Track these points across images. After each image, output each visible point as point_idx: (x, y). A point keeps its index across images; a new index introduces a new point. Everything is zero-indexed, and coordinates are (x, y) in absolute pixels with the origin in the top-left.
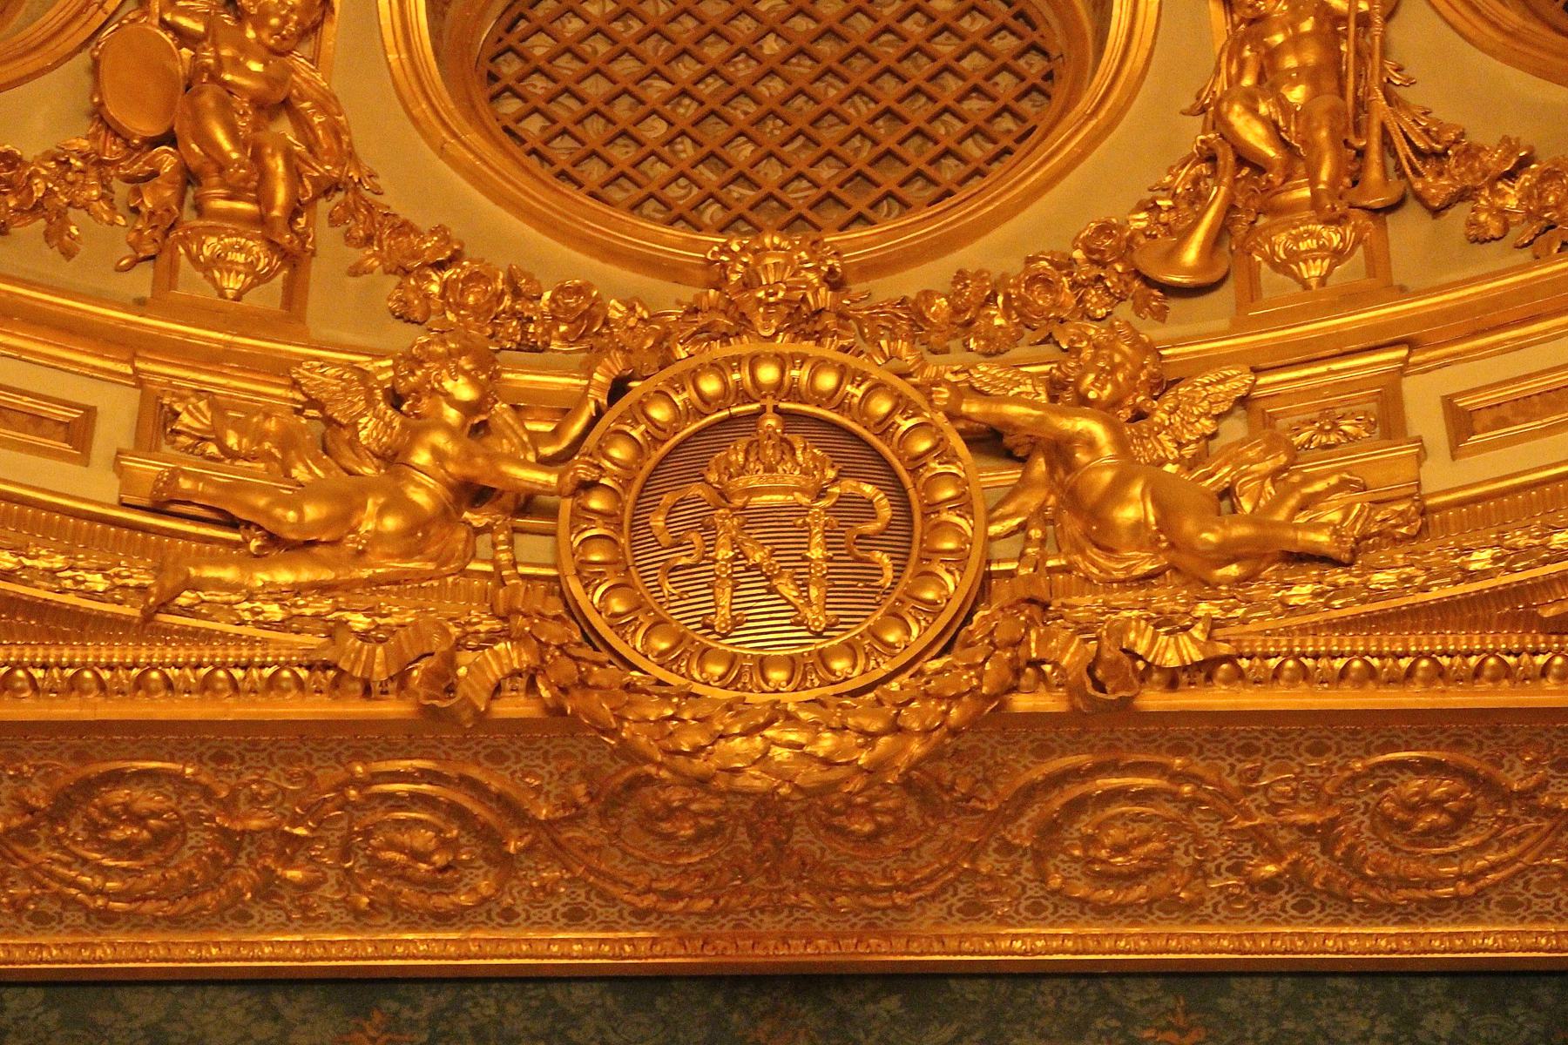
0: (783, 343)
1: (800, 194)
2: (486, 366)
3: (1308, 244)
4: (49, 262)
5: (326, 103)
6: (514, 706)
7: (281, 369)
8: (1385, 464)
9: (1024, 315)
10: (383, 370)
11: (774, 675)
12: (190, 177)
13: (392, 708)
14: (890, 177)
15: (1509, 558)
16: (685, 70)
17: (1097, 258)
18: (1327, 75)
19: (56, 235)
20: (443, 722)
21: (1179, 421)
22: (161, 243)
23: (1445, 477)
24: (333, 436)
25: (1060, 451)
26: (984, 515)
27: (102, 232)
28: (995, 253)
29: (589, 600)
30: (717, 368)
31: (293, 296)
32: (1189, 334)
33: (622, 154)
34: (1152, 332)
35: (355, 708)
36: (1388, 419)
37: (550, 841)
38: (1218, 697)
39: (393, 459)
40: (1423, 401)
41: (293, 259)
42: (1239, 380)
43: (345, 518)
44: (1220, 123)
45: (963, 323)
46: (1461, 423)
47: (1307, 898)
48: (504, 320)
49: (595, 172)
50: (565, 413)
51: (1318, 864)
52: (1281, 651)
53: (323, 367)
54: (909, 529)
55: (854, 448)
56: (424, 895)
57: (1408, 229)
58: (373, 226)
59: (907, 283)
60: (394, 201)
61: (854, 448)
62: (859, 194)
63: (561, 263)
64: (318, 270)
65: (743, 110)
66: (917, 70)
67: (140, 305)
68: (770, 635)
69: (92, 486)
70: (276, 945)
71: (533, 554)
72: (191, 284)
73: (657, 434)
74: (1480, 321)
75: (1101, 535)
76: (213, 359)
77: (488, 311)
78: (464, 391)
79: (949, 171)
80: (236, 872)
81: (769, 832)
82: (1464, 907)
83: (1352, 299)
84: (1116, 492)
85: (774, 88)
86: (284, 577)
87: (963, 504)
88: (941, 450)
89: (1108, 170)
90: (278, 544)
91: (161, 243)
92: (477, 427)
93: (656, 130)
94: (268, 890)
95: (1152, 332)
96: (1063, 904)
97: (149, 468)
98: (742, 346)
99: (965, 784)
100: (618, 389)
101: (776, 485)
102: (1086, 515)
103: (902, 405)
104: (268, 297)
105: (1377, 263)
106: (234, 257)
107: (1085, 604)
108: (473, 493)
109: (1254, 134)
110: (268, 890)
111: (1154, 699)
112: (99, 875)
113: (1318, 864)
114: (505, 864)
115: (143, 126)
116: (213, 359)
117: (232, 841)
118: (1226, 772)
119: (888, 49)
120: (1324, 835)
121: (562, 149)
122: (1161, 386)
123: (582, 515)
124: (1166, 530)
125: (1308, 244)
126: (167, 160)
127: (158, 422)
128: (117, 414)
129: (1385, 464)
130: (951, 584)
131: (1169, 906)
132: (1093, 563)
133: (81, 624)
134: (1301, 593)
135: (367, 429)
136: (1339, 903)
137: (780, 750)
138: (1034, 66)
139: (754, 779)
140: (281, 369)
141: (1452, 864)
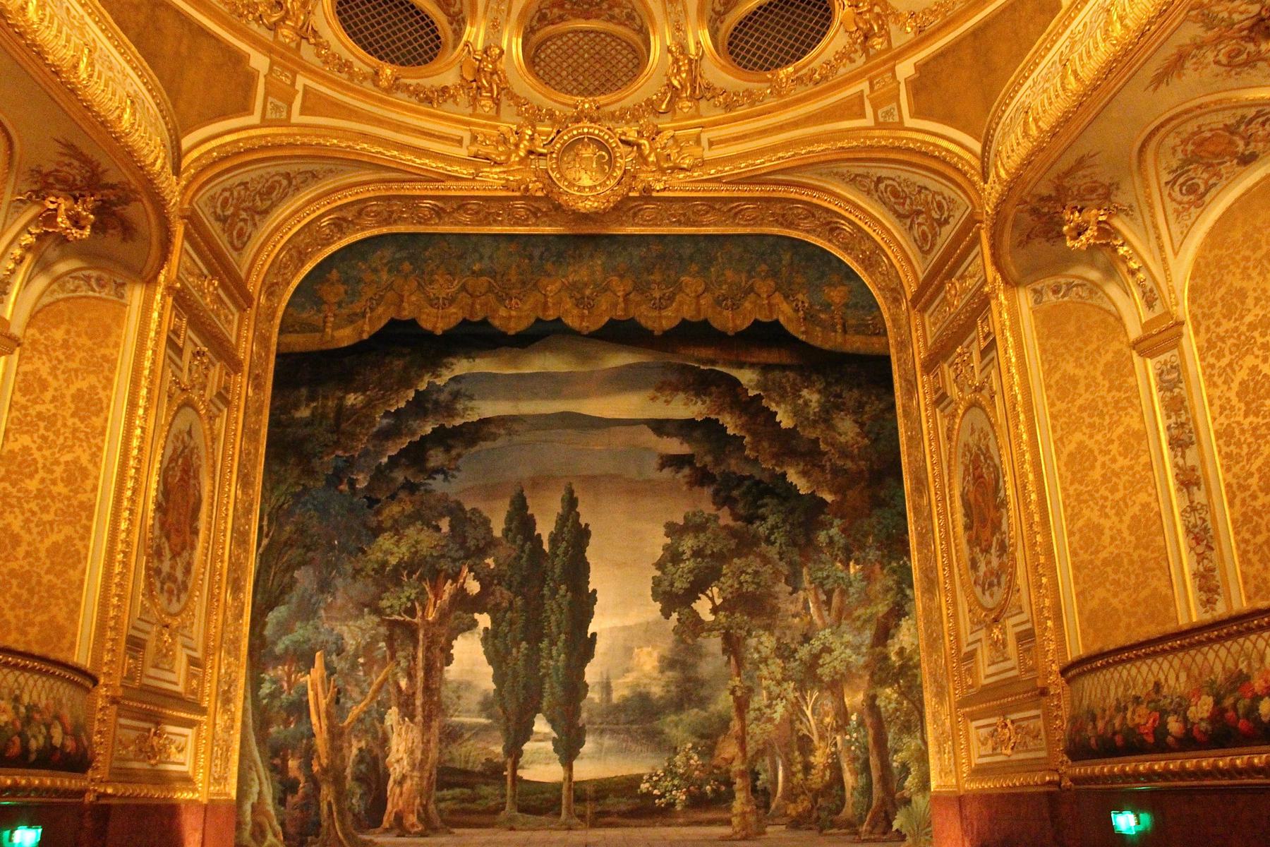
0: (588, 124)
1: (591, 88)
2: (534, 127)
3: (686, 105)
4: (454, 108)
5: (503, 72)
6: (539, 194)
7: (496, 127)
8: (697, 151)
9: (633, 115)
10: (514, 128)
11: (586, 186)
12: (478, 88)
13: (517, 194)
14: (608, 85)
15: (718, 172)
16: (570, 61)
17: (647, 105)
18: (690, 71)
19: (455, 101)
20: (527, 197)
21: (661, 140)
22: (474, 101)
23: (709, 154)
24: (505, 141)
25: (639, 146)
26: (625, 158)
27: (463, 98)
28: (628, 103)
29: (553, 175)
30: (577, 129)
31: (498, 112)
32: (664, 123)
33: (558, 79)
34: (656, 121)
35: (510, 194)
36: (698, 142)
37: (545, 214)
38: (666, 194)
39: (517, 146)
40: (705, 138)
41: (498, 105)
42: (672, 133)
43: (509, 158)
44: (669, 79)
45: (622, 117)
46: (711, 144)
47: (679, 223)
48: (535, 116)
49: (553, 82)
50: (548, 136)
51: (682, 219)
52: (678, 186)
53: (504, 127)
54: (611, 162)
55: (601, 145)
56: (523, 223)
57: (703, 103)
58: (513, 97)
59: (611, 108)
60: (516, 91)
61: (601, 145)
62: (601, 89)
63: (548, 104)
64: (503, 106)
65: (581, 70)
66: (614, 62)
67: (471, 115)
68: (586, 181)
69: (462, 153)
70: (497, 229)
71: (543, 164)
72: (479, 111)
73: (565, 141)
74: (716, 124)
75: (646, 162)
76: (484, 126)
77: (533, 114)
78: (529, 132)
79: (619, 84)
80: (487, 219)
81: (586, 217)
82: (707, 225)
83: (692, 117)
84: (649, 155)
85: (587, 65)
86: (498, 170)
87: (621, 157)
88: (617, 146)
89: (647, 87)
90: (497, 164)
91: (474, 101)
92: (532, 139)
93: (564, 73)
94: (495, 221)
95: (656, 121)
96: (637, 225)
97: (474, 149)
98: (581, 125)
99: (623, 208)
100: (558, 132)
101: (587, 152)
102: (642, 158)
103: (610, 137)
104: (493, 113)
105: (697, 109)
106: (486, 105)
107: (642, 176)
108: (531, 152)
109: (676, 83)
110: (495, 221)
111: (654, 194)
112: (467, 218)
113: (682, 219)
114: (537, 218)
115: (470, 79)
116: (484, 126)
117: (489, 214)
118: (668, 205)
119: (609, 58)
120: (684, 215)
121: (547, 77)
122: (658, 133)
123: (551, 159)
124: (657, 163)
125: (686, 105)
126: (474, 85)
127: (474, 138)
128: (466, 141)
129: (697, 151)
130: (618, 173)
131: (656, 225)
132: (645, 168)
133: (457, 179)
134: (681, 176)
135: (512, 140)
136: (686, 224)
137: (588, 205)
138: (636, 61)
139: (583, 211)
140: (496, 127)
141: (705, 219)
